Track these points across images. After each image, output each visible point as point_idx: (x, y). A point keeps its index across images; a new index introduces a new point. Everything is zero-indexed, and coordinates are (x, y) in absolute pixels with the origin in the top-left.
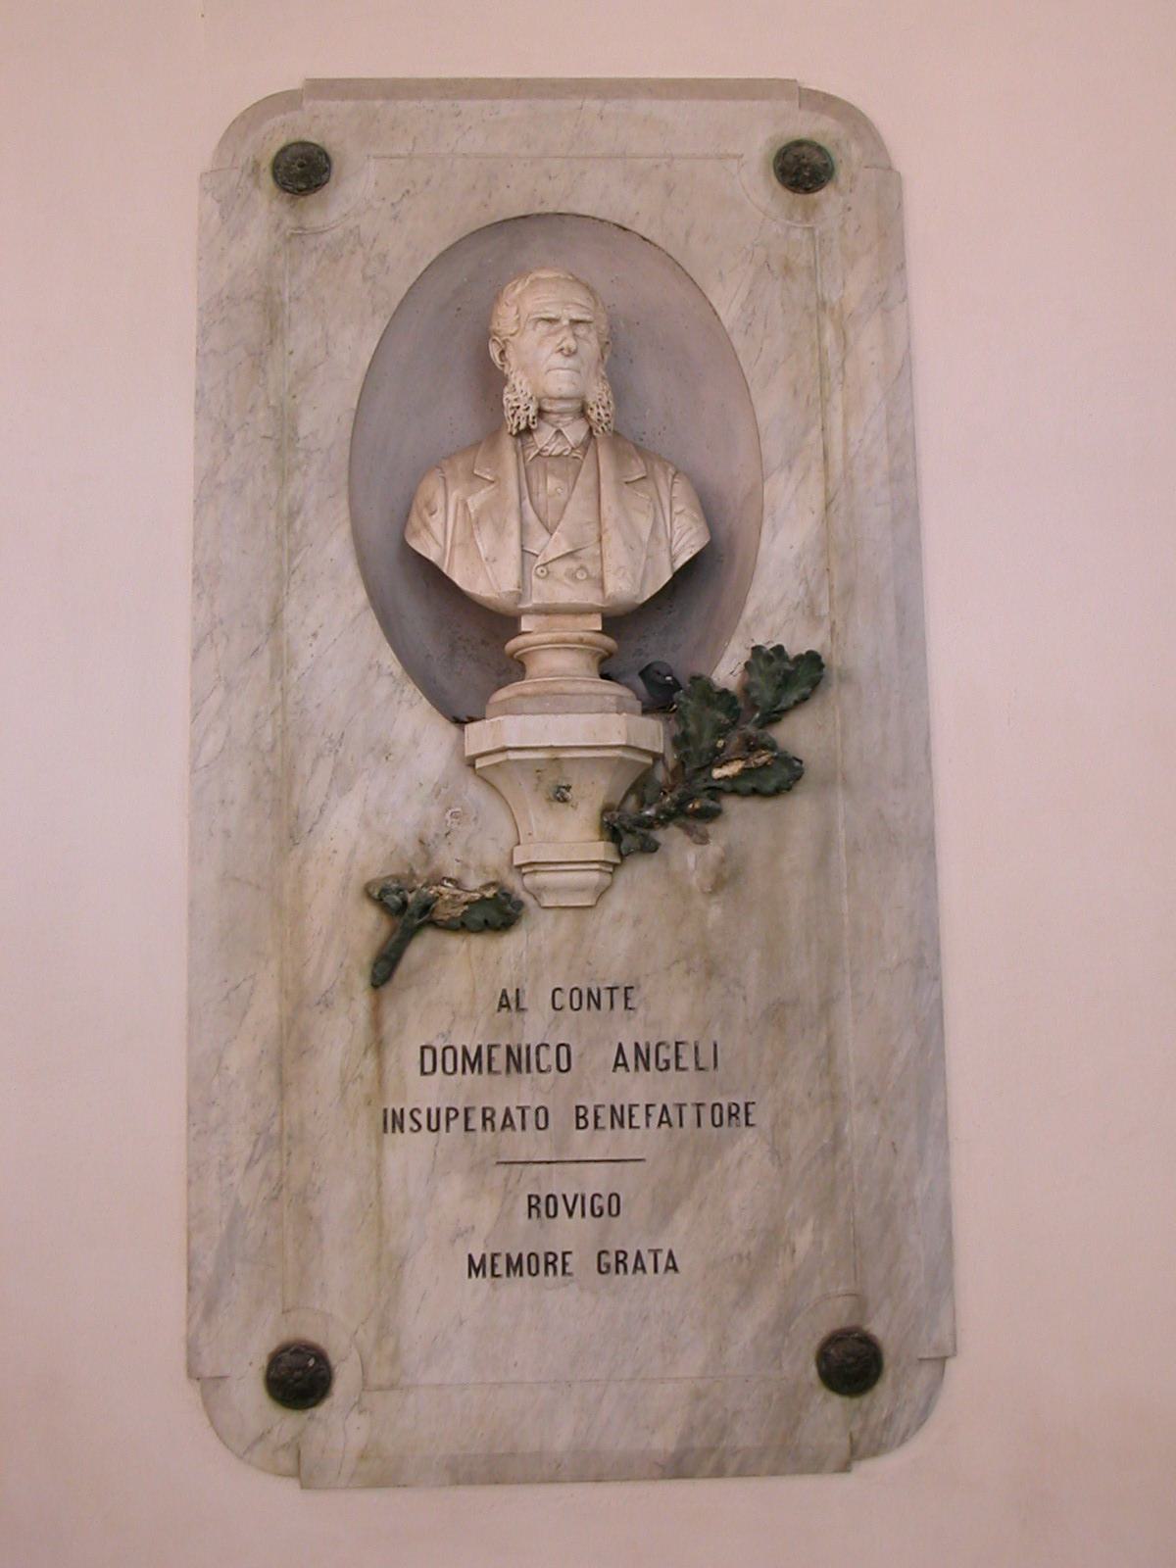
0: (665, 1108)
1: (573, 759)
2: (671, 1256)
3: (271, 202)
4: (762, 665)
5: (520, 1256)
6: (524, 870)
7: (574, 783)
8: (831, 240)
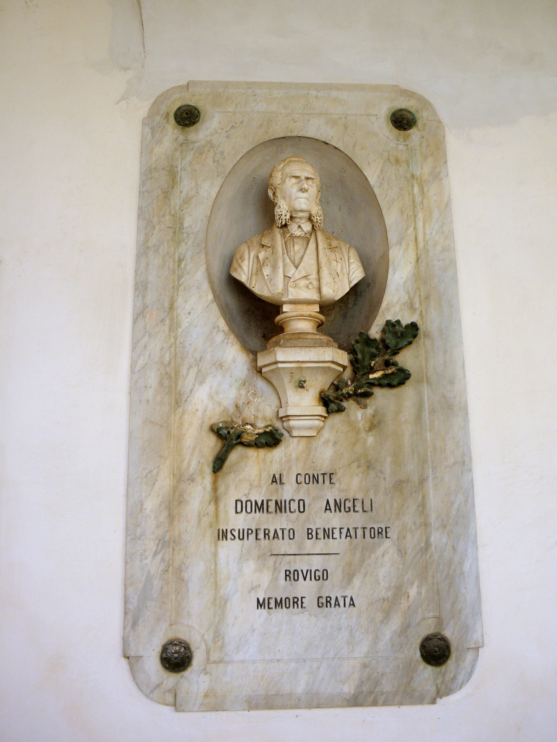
0: (348, 529)
1: (307, 367)
2: (352, 599)
3: (174, 129)
4: (391, 329)
5: (281, 599)
6: (284, 419)
7: (307, 379)
8: (416, 150)
